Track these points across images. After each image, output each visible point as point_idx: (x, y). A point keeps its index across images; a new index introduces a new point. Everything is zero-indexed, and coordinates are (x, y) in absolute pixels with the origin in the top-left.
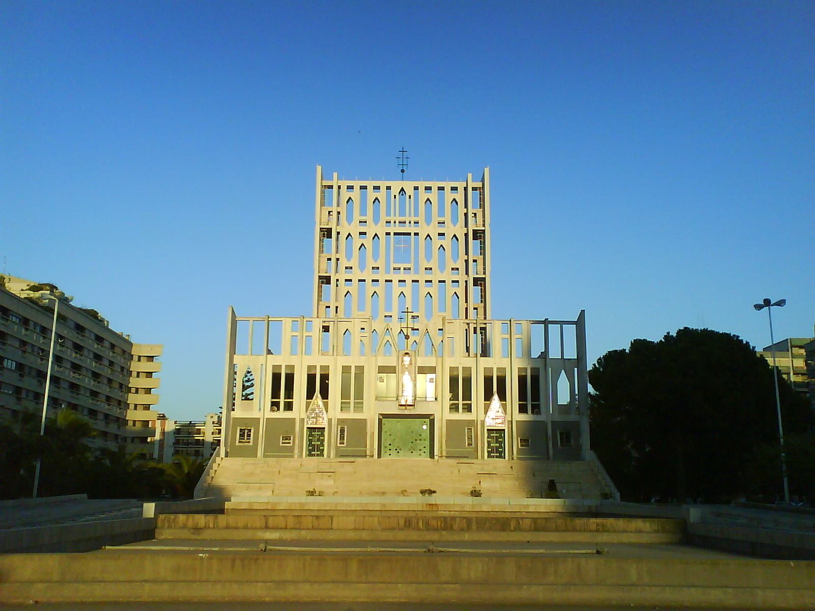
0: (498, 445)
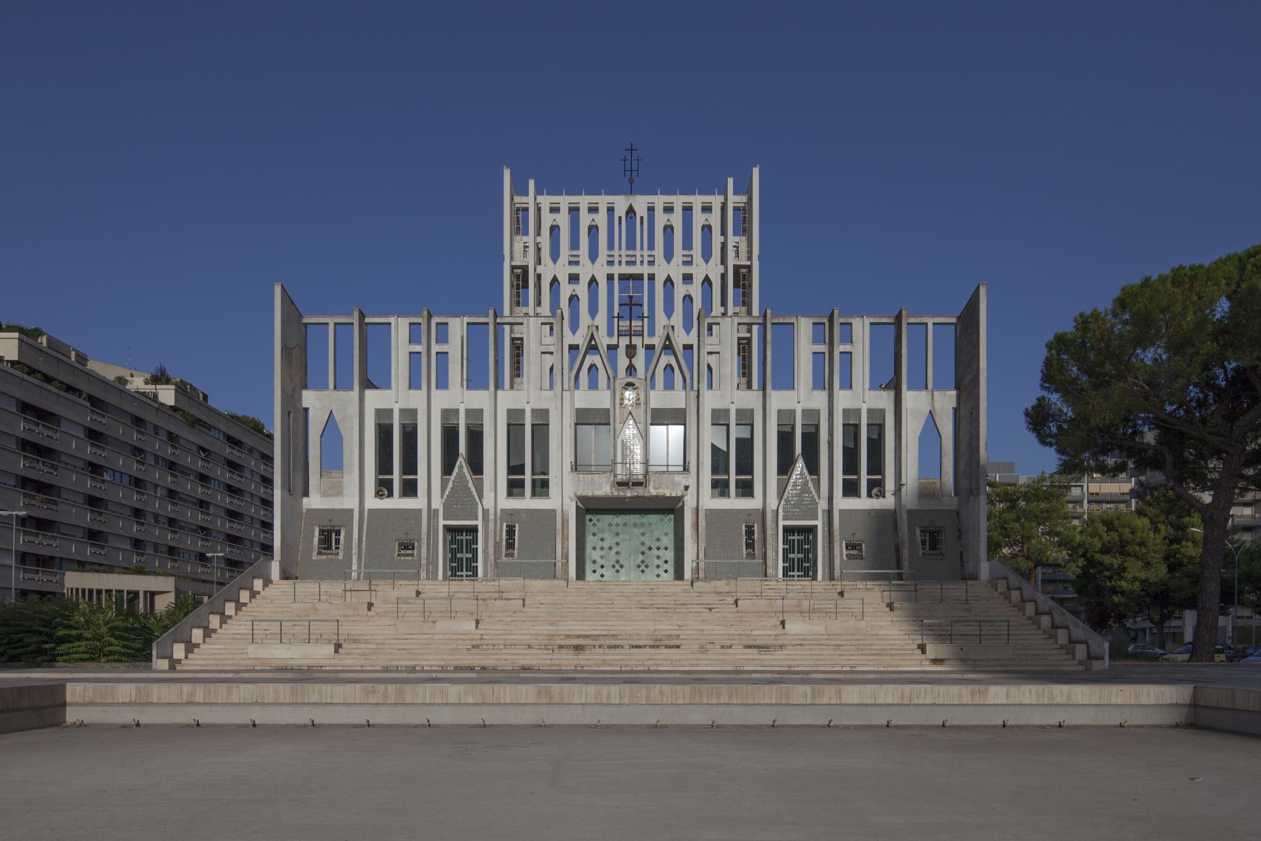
0: (459, 555)
